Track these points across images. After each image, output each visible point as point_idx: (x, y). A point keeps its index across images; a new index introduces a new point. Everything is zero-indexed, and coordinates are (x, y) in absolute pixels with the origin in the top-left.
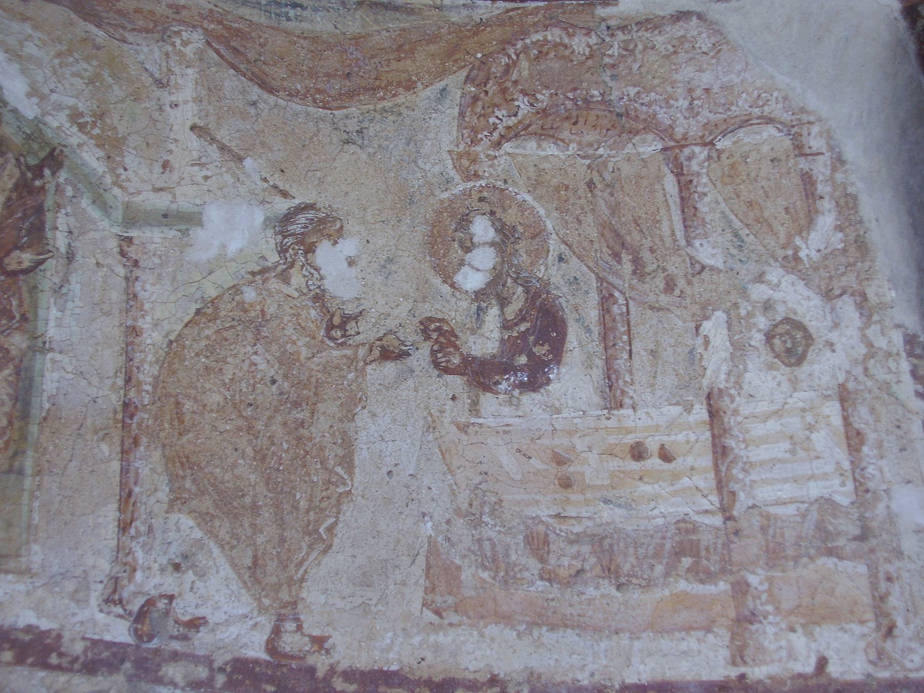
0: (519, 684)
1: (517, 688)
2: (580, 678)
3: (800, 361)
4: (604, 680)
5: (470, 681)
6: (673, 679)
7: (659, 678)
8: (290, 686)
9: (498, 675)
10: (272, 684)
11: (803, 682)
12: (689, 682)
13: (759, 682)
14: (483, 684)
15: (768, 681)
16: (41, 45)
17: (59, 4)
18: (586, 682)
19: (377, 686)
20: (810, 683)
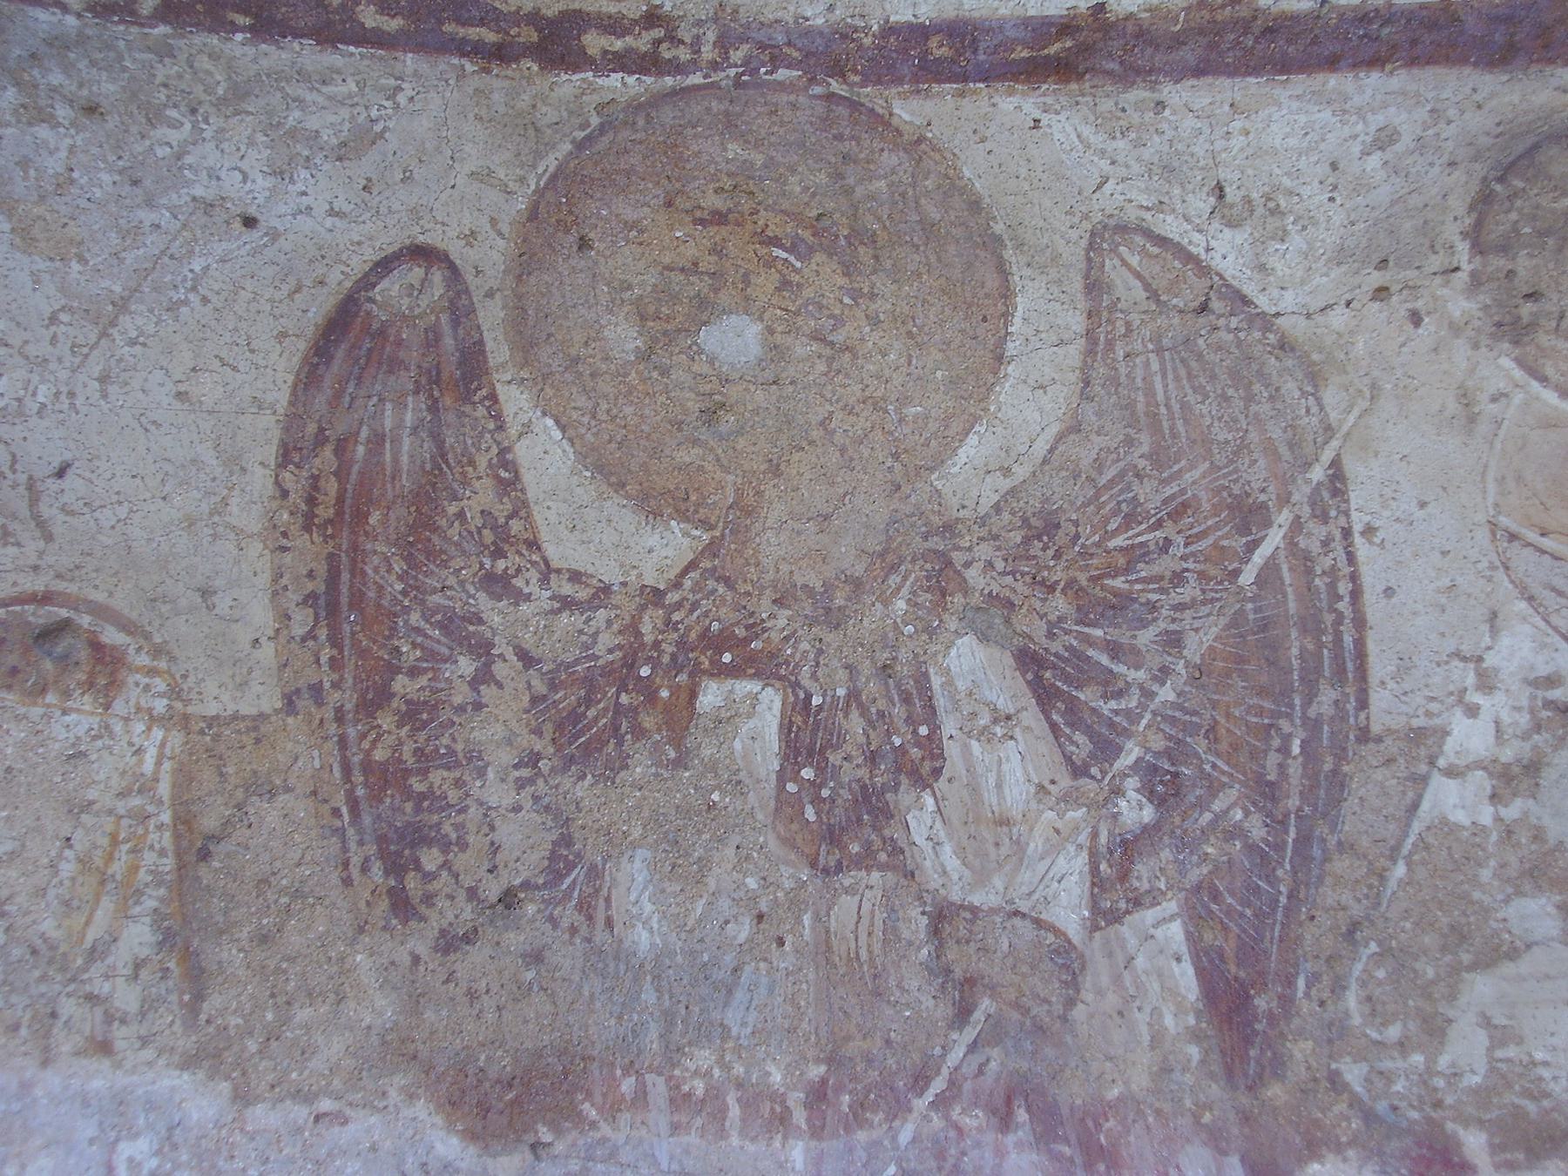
0: (699, 23)
1: (695, 31)
2: (809, 14)
3: (1455, 998)
4: (852, 17)
5: (610, 17)
6: (976, 14)
7: (950, 13)
8: (279, 16)
9: (661, 6)
10: (246, 13)
11: (1207, 17)
12: (1004, 19)
13: (1130, 17)
14: (635, 22)
15: (1145, 15)
16: (325, 512)
17: (329, 34)
18: (820, 21)
19: (440, 22)
20: (1219, 18)
